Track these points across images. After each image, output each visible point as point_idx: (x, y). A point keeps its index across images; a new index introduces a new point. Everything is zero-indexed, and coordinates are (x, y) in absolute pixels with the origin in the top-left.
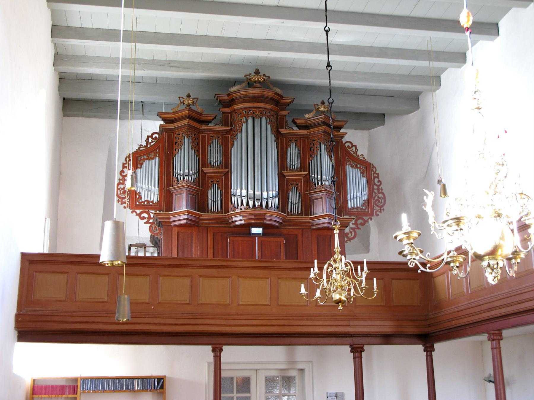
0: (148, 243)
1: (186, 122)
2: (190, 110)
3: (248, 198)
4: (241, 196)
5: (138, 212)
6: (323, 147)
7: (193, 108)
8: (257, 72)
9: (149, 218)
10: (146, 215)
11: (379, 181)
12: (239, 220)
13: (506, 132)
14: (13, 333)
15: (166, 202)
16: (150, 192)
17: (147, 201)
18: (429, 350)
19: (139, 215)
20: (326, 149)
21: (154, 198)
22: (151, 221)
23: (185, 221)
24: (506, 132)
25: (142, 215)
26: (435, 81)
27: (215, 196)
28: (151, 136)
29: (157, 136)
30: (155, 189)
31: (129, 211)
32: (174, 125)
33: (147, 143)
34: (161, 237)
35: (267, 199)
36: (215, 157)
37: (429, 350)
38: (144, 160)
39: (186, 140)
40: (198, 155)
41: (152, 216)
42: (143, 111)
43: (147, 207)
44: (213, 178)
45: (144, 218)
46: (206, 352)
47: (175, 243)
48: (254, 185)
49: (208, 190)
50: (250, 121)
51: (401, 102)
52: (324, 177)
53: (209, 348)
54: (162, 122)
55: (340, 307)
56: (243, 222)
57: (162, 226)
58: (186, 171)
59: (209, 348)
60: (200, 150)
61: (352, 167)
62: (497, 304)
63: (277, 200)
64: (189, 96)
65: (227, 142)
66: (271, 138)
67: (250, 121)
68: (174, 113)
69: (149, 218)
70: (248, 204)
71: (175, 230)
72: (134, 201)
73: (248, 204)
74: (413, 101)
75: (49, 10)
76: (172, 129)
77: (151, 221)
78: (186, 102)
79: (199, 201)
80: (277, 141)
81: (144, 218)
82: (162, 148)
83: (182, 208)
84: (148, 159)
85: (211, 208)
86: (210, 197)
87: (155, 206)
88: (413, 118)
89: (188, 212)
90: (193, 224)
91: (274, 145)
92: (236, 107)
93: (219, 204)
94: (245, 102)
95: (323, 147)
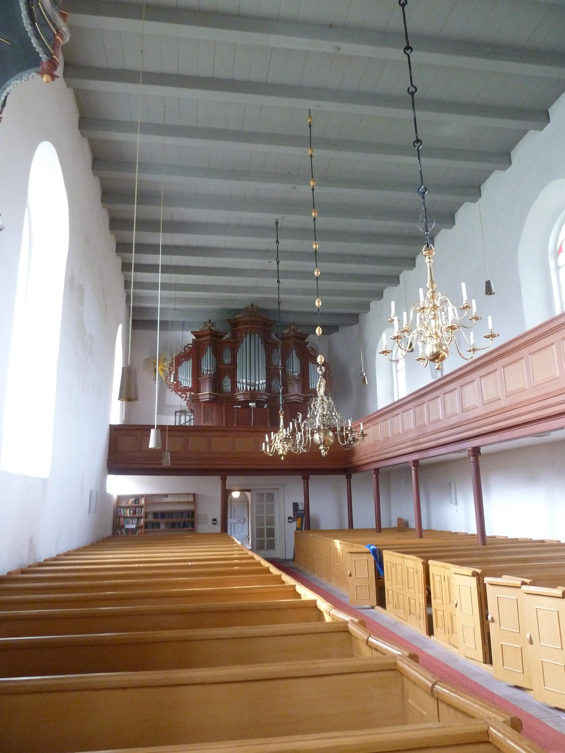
0: (187, 408)
1: (208, 338)
2: (211, 330)
3: (247, 384)
4: (242, 383)
5: (180, 393)
6: (294, 351)
7: (213, 328)
8: (252, 305)
9: (186, 397)
10: (184, 395)
11: (330, 372)
12: (241, 398)
13: (489, 290)
14: (399, 517)
15: (197, 387)
16: (187, 381)
17: (185, 386)
18: (349, 478)
19: (180, 395)
20: (296, 352)
21: (189, 385)
22: (188, 399)
23: (208, 399)
24: (489, 290)
25: (182, 395)
26: (366, 307)
27: (227, 385)
28: (187, 346)
29: (191, 346)
30: (190, 379)
31: (174, 393)
32: (201, 339)
33: (185, 351)
34: (193, 409)
35: (258, 385)
36: (227, 360)
37: (349, 478)
38: (183, 361)
39: (209, 349)
40: (216, 358)
41: (188, 396)
42: (183, 326)
43: (185, 390)
44: (224, 372)
45: (183, 397)
46: (217, 480)
47: (202, 412)
48: (250, 378)
49: (222, 379)
50: (248, 336)
51: (348, 319)
52: (294, 370)
53: (219, 477)
54: (195, 338)
55: (282, 458)
56: (243, 399)
57: (194, 401)
58: (209, 368)
59: (219, 477)
60: (217, 355)
61: (313, 363)
62: (373, 454)
63: (265, 385)
64: (210, 321)
65: (234, 346)
66: (261, 347)
67: (248, 336)
68: (201, 332)
69: (186, 397)
70: (247, 387)
71: (202, 406)
72: (178, 388)
73: (247, 387)
74: (354, 319)
75: (97, 178)
76: (200, 342)
77: (188, 399)
78: (208, 325)
79: (216, 385)
80: (265, 348)
81: (183, 397)
82: (194, 353)
83: (206, 393)
84: (186, 360)
85: (225, 390)
86: (224, 384)
87: (190, 390)
88: (355, 328)
89: (210, 394)
90: (214, 400)
91: (263, 350)
92: (240, 327)
93: (229, 388)
94: (245, 324)
95: (294, 351)
